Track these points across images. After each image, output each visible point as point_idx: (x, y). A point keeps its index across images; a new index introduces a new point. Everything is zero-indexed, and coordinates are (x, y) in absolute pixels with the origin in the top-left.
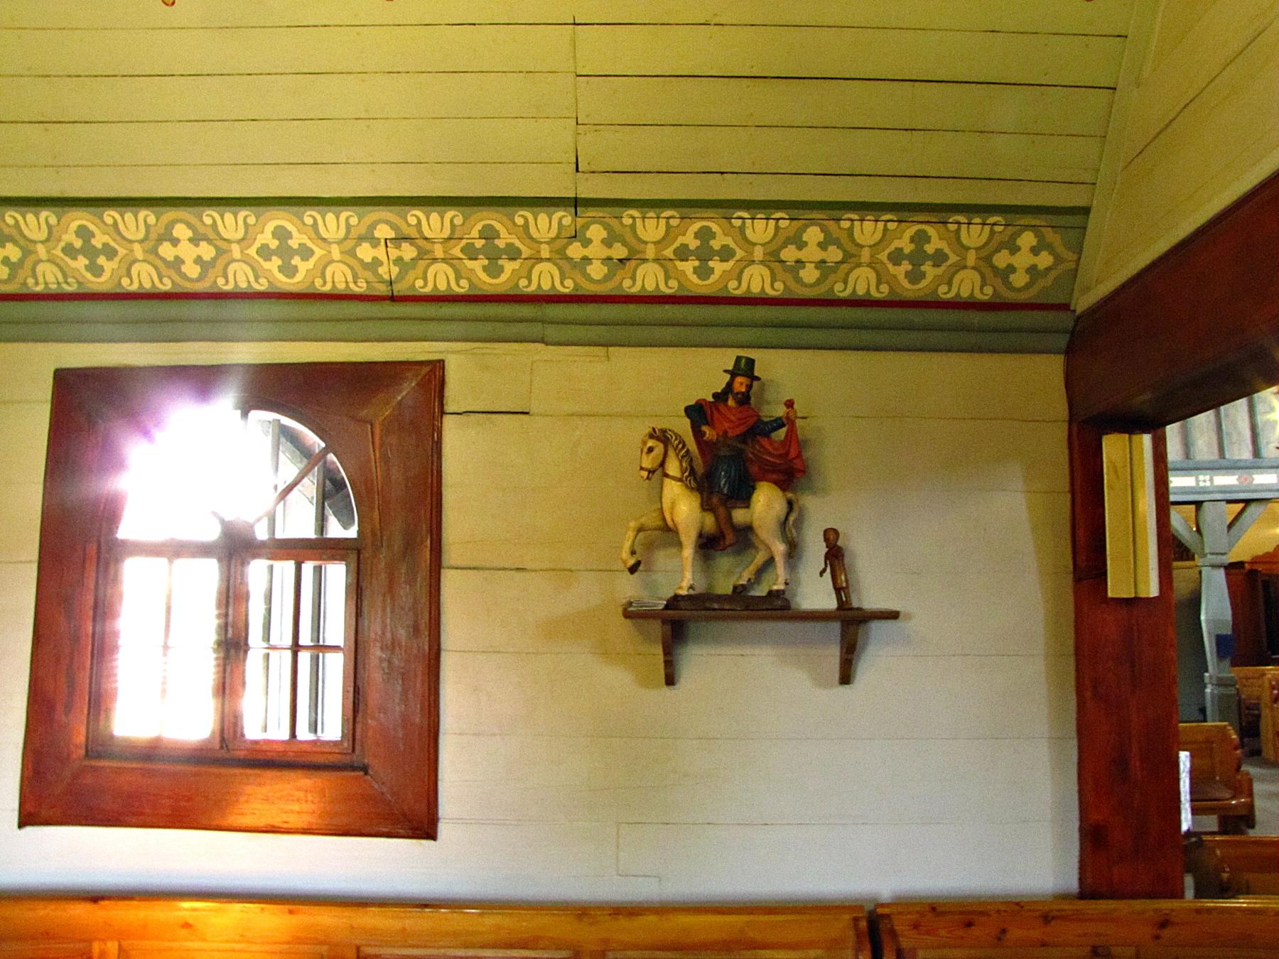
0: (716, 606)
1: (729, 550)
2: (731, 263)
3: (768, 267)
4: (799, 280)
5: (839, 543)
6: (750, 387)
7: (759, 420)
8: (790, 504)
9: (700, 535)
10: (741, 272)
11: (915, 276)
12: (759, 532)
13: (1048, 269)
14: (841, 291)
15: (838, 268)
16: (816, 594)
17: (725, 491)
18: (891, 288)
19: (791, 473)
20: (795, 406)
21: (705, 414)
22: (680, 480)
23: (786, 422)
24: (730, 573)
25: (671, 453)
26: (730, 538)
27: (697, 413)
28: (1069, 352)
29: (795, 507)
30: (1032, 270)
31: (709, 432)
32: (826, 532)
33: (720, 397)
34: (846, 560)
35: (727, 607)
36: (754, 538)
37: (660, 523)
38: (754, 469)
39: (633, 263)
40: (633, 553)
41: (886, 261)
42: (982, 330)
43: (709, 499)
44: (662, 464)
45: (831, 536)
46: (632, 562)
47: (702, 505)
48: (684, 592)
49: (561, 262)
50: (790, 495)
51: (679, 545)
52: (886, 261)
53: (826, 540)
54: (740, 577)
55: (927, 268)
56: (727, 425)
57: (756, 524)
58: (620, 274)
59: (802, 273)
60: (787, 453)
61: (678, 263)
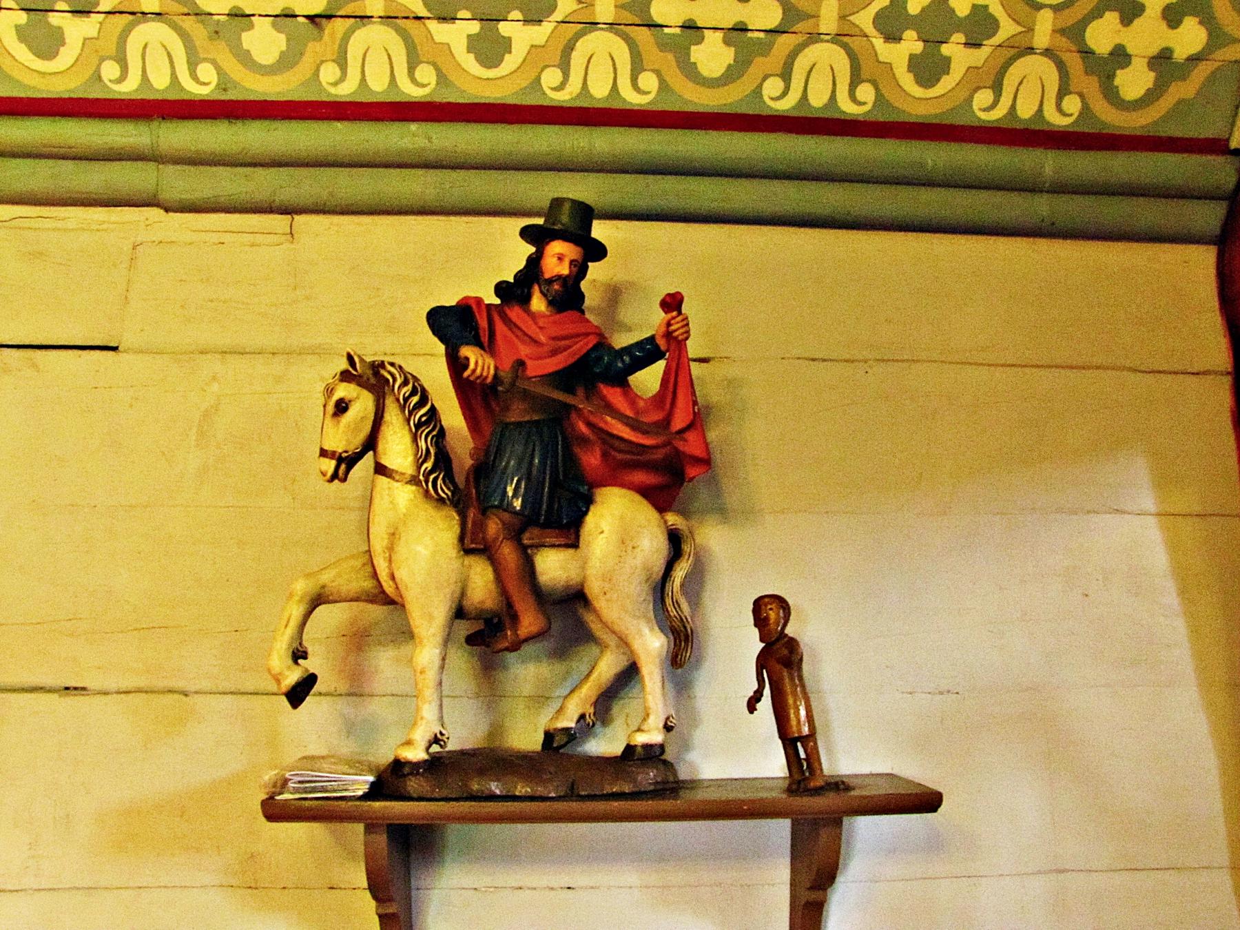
0: (495, 788)
1: (527, 649)
2: (547, 27)
3: (627, 39)
4: (690, 71)
5: (790, 631)
6: (580, 270)
7: (602, 344)
8: (675, 540)
9: (460, 613)
10: (569, 48)
11: (928, 68)
12: (600, 603)
13: (1194, 59)
14: (778, 98)
15: (770, 46)
16: (736, 747)
17: (518, 504)
18: (879, 96)
19: (674, 472)
20: (685, 308)
21: (476, 328)
22: (414, 481)
23: (665, 346)
24: (540, 699)
25: (393, 415)
26: (529, 622)
27: (454, 324)
28: (1222, 241)
29: (686, 548)
30: (1161, 59)
31: (477, 360)
32: (759, 605)
33: (513, 292)
34: (806, 667)
35: (521, 789)
36: (589, 618)
37: (368, 584)
38: (591, 460)
39: (339, 26)
40: (299, 655)
41: (869, 29)
42: (1060, 189)
43: (480, 526)
44: (371, 443)
45: (769, 614)
46: (293, 677)
47: (461, 539)
48: (416, 754)
49: (189, 23)
50: (672, 518)
51: (406, 634)
52: (869, 29)
53: (760, 621)
54: (560, 711)
55: (953, 49)
56: (524, 351)
57: (594, 589)
58: (313, 50)
59: (698, 54)
60: (667, 421)
61: (433, 25)
